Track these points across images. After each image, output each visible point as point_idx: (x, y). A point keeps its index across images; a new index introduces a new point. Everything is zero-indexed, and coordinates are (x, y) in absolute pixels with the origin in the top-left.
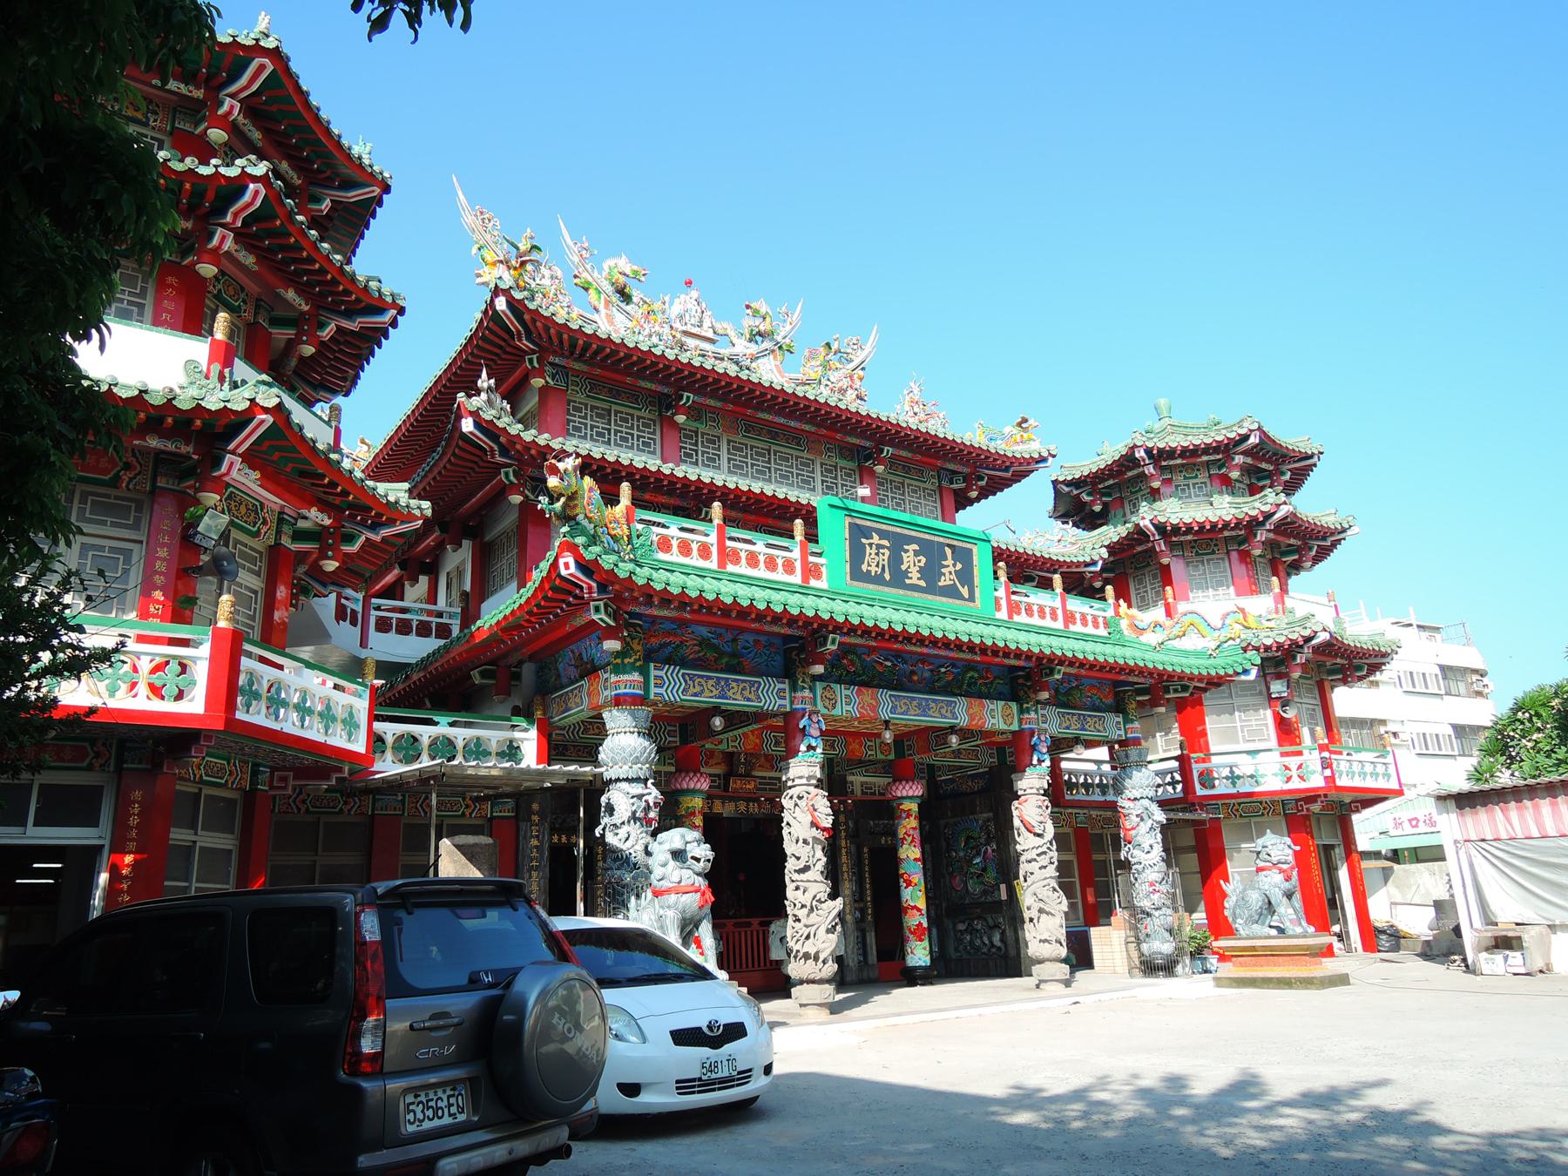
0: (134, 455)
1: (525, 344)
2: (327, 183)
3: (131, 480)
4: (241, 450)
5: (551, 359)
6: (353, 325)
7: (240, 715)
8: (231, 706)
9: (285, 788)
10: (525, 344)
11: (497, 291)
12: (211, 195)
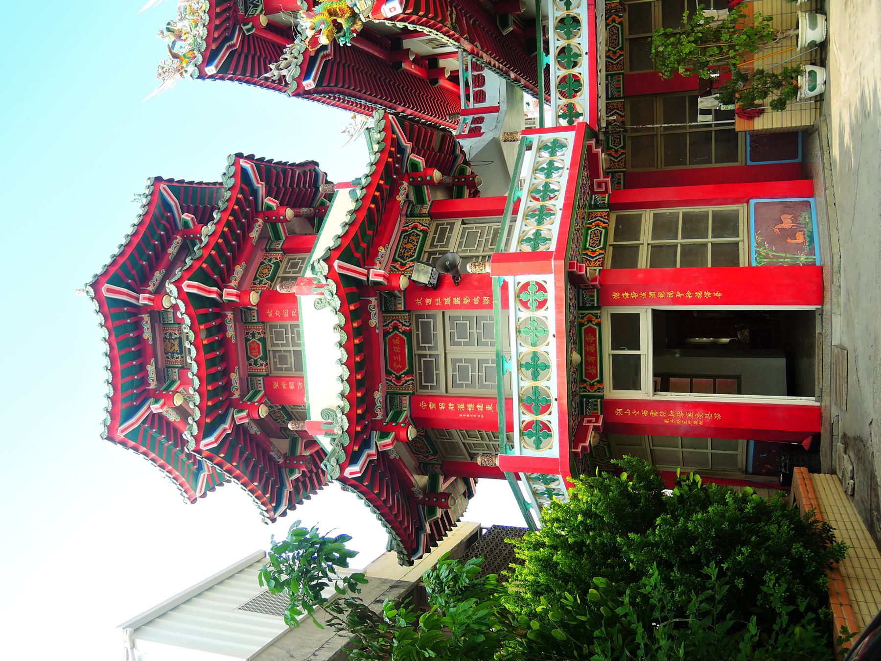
0: (387, 325)
1: (236, 40)
2: (172, 221)
3: (403, 325)
4: (365, 271)
5: (241, 12)
6: (261, 187)
7: (553, 247)
8: (547, 256)
9: (606, 183)
10: (236, 40)
11: (202, 76)
12: (202, 311)
